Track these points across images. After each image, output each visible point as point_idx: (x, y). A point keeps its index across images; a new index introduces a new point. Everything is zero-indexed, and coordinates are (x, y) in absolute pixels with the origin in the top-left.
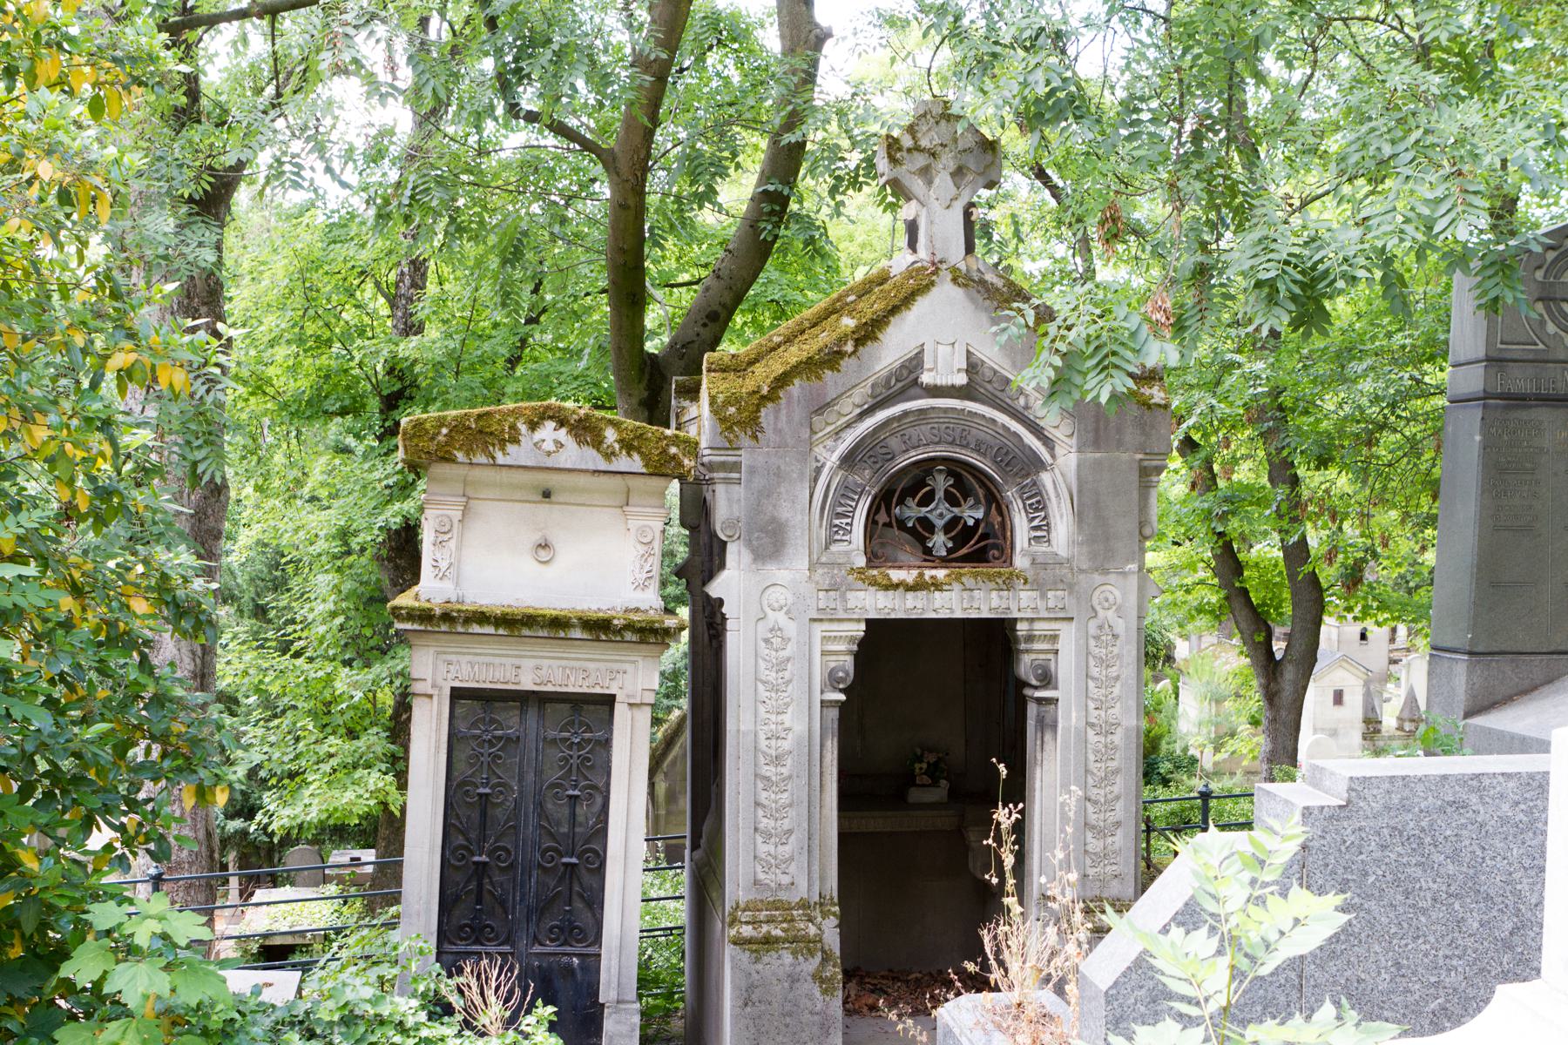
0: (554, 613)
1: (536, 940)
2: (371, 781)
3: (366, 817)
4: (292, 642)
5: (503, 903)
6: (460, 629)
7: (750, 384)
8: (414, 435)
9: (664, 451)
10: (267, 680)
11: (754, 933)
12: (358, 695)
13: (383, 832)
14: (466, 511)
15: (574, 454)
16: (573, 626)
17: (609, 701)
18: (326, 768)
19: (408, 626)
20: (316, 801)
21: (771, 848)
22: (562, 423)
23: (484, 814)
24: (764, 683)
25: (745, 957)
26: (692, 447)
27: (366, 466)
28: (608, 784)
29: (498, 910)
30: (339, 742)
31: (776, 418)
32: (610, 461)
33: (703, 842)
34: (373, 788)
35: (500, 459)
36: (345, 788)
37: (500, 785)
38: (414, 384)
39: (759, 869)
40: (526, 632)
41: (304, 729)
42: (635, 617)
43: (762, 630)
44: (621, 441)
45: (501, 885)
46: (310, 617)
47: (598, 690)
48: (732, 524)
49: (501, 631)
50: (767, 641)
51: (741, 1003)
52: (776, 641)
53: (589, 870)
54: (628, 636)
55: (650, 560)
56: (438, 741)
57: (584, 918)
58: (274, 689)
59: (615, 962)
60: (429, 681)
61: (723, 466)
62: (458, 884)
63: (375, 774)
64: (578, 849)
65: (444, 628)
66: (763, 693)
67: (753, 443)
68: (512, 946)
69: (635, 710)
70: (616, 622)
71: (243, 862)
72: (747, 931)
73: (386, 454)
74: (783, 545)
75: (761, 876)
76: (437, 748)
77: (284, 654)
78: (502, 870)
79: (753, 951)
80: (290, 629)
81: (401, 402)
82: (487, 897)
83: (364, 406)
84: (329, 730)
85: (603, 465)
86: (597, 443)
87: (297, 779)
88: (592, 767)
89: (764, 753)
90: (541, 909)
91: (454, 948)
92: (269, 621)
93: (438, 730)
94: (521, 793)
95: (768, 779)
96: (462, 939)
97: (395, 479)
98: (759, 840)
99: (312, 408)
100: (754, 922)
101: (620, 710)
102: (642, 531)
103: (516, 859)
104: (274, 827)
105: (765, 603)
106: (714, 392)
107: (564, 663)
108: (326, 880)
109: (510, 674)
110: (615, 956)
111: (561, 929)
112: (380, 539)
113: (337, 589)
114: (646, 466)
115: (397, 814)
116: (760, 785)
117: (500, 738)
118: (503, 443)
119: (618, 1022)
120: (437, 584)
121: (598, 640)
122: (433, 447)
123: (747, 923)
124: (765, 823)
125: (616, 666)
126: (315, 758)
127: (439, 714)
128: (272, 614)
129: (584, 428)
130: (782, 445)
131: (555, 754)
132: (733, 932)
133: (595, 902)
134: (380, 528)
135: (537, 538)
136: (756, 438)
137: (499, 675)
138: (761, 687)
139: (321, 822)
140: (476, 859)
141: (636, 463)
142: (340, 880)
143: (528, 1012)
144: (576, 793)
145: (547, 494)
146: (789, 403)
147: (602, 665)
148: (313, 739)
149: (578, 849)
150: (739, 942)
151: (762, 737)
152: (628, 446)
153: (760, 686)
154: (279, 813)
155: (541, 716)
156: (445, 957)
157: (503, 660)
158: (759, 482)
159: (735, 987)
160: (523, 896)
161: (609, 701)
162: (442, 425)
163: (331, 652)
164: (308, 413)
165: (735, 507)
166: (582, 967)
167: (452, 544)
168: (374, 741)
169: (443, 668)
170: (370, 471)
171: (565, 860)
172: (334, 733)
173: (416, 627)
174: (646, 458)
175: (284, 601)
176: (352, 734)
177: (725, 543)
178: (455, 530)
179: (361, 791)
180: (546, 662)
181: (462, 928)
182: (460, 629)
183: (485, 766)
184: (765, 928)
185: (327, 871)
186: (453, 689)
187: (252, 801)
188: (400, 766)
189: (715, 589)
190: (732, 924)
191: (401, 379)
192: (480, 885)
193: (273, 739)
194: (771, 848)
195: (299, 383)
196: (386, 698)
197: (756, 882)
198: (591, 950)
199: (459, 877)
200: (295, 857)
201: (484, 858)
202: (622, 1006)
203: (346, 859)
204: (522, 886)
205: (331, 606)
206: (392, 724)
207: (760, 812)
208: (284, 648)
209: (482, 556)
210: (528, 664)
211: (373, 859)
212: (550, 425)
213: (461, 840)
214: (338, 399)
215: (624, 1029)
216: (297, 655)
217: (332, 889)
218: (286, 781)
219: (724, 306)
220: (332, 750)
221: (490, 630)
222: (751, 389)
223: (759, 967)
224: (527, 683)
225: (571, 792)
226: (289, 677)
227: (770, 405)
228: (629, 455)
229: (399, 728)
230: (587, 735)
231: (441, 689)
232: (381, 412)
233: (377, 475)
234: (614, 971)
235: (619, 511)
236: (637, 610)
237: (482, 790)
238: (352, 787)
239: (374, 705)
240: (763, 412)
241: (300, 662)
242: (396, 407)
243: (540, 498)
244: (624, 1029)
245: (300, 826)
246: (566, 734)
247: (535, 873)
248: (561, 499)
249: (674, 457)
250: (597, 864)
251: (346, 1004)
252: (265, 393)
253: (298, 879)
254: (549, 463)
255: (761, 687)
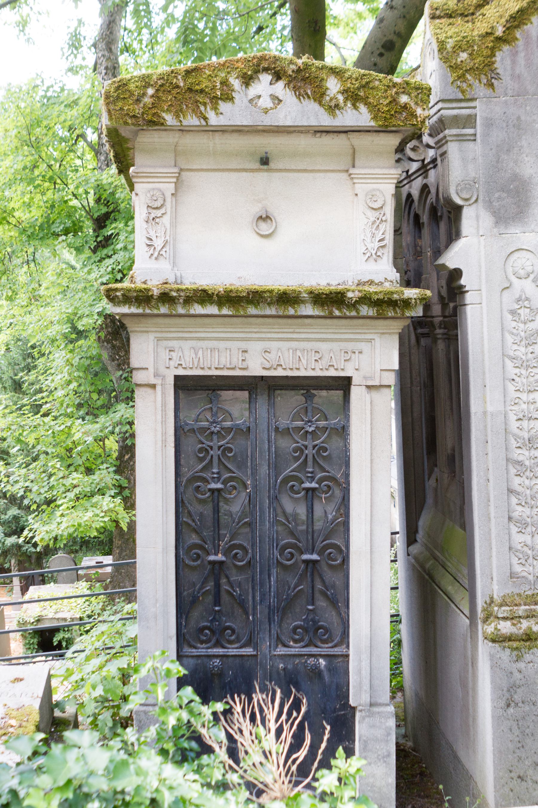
0: (282, 288)
1: (280, 641)
2: (105, 503)
3: (103, 531)
4: (41, 406)
5: (242, 604)
6: (181, 310)
7: (481, 27)
8: (118, 97)
9: (394, 101)
10: (25, 433)
11: (514, 630)
12: (90, 439)
13: (117, 542)
14: (178, 183)
15: (294, 110)
16: (303, 302)
17: (344, 384)
18: (71, 495)
19: (125, 309)
20: (65, 519)
21: (528, 539)
22: (278, 76)
23: (216, 510)
24: (512, 359)
25: (505, 655)
26: (423, 92)
27: (86, 270)
28: (347, 475)
29: (238, 611)
30: (81, 476)
31: (514, 62)
32: (334, 116)
33: (420, 536)
34: (105, 508)
35: (214, 119)
36: (87, 510)
37: (231, 479)
38: (116, 210)
39: (515, 561)
40: (252, 310)
41: (53, 467)
42: (373, 289)
43: (508, 298)
44: (344, 92)
45: (240, 585)
46: (53, 386)
47: (332, 373)
48: (469, 185)
49: (225, 311)
50: (513, 312)
51: (503, 704)
52: (524, 313)
53: (331, 567)
54: (365, 310)
55: (382, 227)
56: (164, 434)
57: (328, 617)
58: (31, 440)
59: (365, 665)
60: (151, 370)
61: (456, 121)
62: (194, 585)
63: (107, 499)
64: (319, 545)
65: (164, 309)
66: (511, 371)
67: (489, 91)
68: (255, 648)
69: (375, 394)
70: (350, 295)
71: (21, 566)
72: (506, 627)
73: (100, 261)
74: (528, 205)
75: (518, 569)
76: (164, 442)
77: (37, 414)
78: (240, 569)
79: (513, 649)
80: (39, 396)
81: (108, 222)
82: (225, 598)
83: (81, 228)
84: (72, 468)
85: (325, 120)
86: (319, 95)
87: (52, 505)
88: (329, 456)
89: (516, 437)
90: (283, 608)
91: (194, 652)
92: (24, 393)
93: (164, 422)
94: (255, 487)
95: (520, 463)
96: (202, 642)
97: (107, 277)
98: (514, 529)
99: (43, 232)
100: (512, 618)
101: (357, 393)
102: (372, 195)
103: (254, 557)
104: (37, 539)
105: (510, 271)
106: (442, 37)
107: (294, 344)
108: (79, 578)
109: (236, 359)
110: (365, 657)
111: (306, 630)
112: (99, 322)
113: (68, 362)
114: (375, 118)
115: (125, 529)
116: (513, 471)
117: (229, 430)
118: (215, 100)
119: (373, 726)
120: (153, 265)
121: (331, 317)
122: (138, 110)
123: (505, 619)
124: (518, 511)
125: (350, 346)
126: (63, 489)
127: (164, 404)
128: (25, 386)
129: (304, 79)
130: (520, 93)
131: (287, 445)
132: (490, 629)
133: (340, 600)
134: (99, 314)
135: (257, 210)
136: (491, 85)
137: (224, 361)
138: (509, 364)
139: (70, 535)
140: (212, 558)
141: (362, 117)
142: (88, 579)
143: (326, 765)
144: (314, 485)
145: (265, 161)
146: (527, 43)
147: (335, 346)
148: (61, 474)
149: (319, 545)
150: (497, 639)
151: (512, 418)
152: (354, 97)
153: (508, 362)
154: (42, 530)
155: (271, 404)
156: (185, 660)
157: (229, 344)
158: (497, 135)
159: (496, 687)
160: (263, 595)
161: (344, 384)
162: (148, 85)
163: (69, 410)
164: (41, 235)
165: (471, 167)
166: (330, 669)
167: (166, 220)
168: (105, 475)
169: (164, 355)
170: (89, 273)
171: (305, 557)
172: (76, 470)
173: (134, 310)
174: (376, 114)
175: (32, 376)
176: (89, 471)
177: (459, 209)
178: (168, 204)
179: (98, 512)
180: (274, 345)
181: (201, 630)
182: (181, 310)
183: (215, 461)
184: (525, 624)
185: (80, 572)
186: (177, 378)
187: (21, 523)
188: (127, 493)
189: (452, 258)
190: (486, 620)
191: (107, 205)
192: (218, 586)
193: (32, 477)
194: (528, 539)
195: (32, 214)
196: (112, 445)
197: (512, 575)
198: (337, 651)
199: (194, 577)
200: (57, 562)
201: (220, 557)
202: (376, 709)
203: (93, 563)
204: (262, 585)
205: (67, 377)
206: (118, 463)
207: (514, 500)
208: (36, 408)
209: (200, 230)
210: (255, 348)
211: (111, 562)
212: (266, 78)
213: (194, 539)
214: (61, 223)
215: (379, 733)
216: (45, 415)
217: (83, 587)
218: (44, 507)
219: (398, 34)
220: (75, 482)
221: (213, 310)
222: (483, 31)
223: (521, 665)
224: (256, 368)
225: (307, 485)
226: (39, 431)
227: (506, 48)
228: (355, 107)
229: (125, 461)
230: (322, 423)
231: (164, 378)
232: (94, 231)
233: (93, 276)
234: (365, 672)
235: (345, 176)
236: (371, 282)
237: (213, 486)
238: (91, 509)
239: (104, 449)
240: (499, 56)
241: (46, 419)
242: (105, 226)
243: (257, 165)
244: (379, 733)
245: (56, 539)
246: (300, 423)
247: (274, 571)
248: (281, 166)
249: (405, 107)
250: (339, 560)
251: (69, 782)
252: (8, 223)
253: (60, 578)
254: (268, 121)
255: (509, 364)
